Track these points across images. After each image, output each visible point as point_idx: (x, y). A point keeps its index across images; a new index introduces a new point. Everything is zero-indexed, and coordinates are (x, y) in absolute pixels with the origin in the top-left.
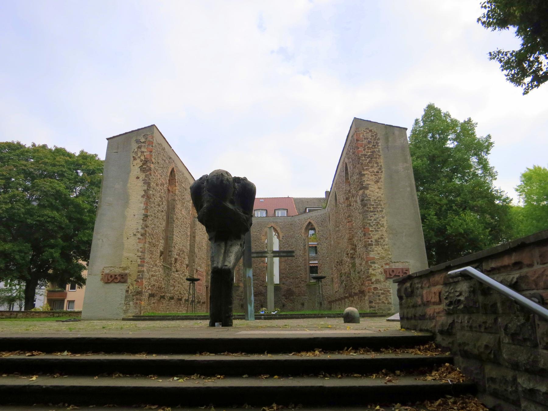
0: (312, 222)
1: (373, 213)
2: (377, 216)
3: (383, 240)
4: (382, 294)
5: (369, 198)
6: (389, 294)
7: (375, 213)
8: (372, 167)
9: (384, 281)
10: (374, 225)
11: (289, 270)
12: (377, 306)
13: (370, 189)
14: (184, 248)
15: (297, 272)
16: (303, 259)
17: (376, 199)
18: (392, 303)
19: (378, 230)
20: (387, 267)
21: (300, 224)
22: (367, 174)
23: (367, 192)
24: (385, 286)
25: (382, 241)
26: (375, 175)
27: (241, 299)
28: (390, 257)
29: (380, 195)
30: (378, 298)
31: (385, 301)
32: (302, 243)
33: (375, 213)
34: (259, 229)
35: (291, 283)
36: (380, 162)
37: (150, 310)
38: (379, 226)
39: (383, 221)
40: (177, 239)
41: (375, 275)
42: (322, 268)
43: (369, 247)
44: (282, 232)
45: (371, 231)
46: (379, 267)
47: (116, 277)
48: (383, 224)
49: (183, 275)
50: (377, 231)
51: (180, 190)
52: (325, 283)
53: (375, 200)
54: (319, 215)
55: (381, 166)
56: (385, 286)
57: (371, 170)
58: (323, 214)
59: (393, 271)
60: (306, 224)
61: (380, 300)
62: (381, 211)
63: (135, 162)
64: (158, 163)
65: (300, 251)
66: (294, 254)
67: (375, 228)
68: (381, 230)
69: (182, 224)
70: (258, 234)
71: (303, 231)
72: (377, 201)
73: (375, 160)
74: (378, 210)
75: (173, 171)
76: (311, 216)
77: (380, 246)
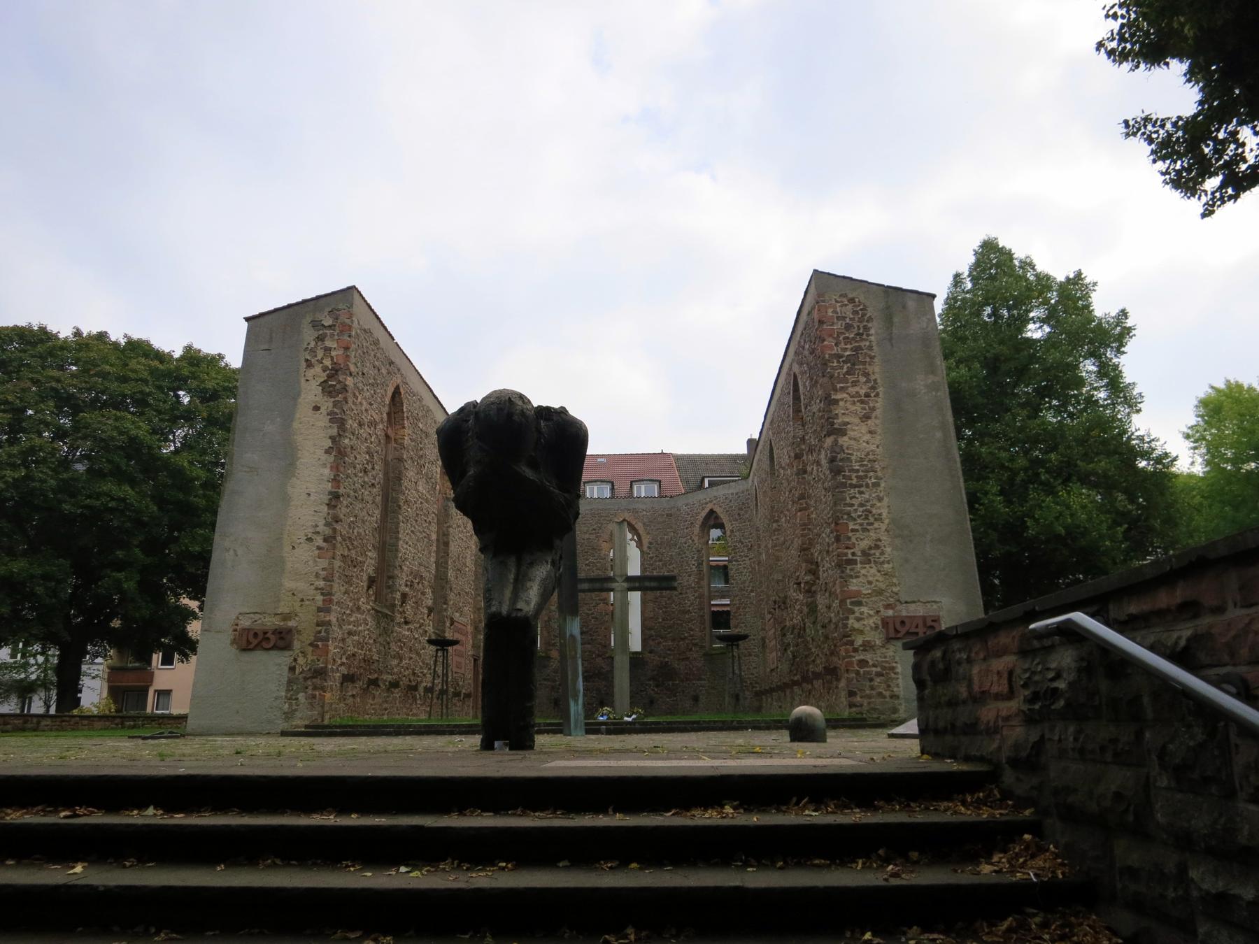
1: (857, 489)
2: (867, 496)
3: (879, 551)
4: (879, 674)
7: (862, 489)
8: (855, 384)
9: (883, 646)
10: (859, 516)
11: (663, 620)
12: (865, 702)
13: (852, 434)
15: (681, 625)
16: (696, 594)
17: (863, 456)
18: (901, 696)
19: (869, 527)
20: (890, 613)
22: (842, 399)
23: (844, 441)
24: (885, 657)
25: (877, 554)
26: (862, 402)
27: (553, 688)
28: (895, 590)
29: (873, 447)
31: (884, 692)
32: (693, 558)
33: (862, 489)
35: (669, 650)
36: (873, 373)
38: (872, 520)
39: (879, 508)
41: (861, 632)
42: (740, 615)
44: (648, 534)
45: (853, 530)
46: (871, 612)
48: (880, 514)
50: (865, 530)
51: (414, 436)
52: (746, 649)
53: (862, 460)
54: (732, 494)
55: (875, 380)
57: (852, 390)
58: (743, 492)
59: (903, 623)
60: (704, 514)
61: (872, 688)
62: (876, 485)
63: (310, 373)
65: (690, 576)
66: (676, 584)
67: (861, 524)
68: (876, 529)
69: (417, 515)
70: (593, 537)
71: (697, 530)
72: (865, 463)
73: (861, 367)
77: (873, 565)
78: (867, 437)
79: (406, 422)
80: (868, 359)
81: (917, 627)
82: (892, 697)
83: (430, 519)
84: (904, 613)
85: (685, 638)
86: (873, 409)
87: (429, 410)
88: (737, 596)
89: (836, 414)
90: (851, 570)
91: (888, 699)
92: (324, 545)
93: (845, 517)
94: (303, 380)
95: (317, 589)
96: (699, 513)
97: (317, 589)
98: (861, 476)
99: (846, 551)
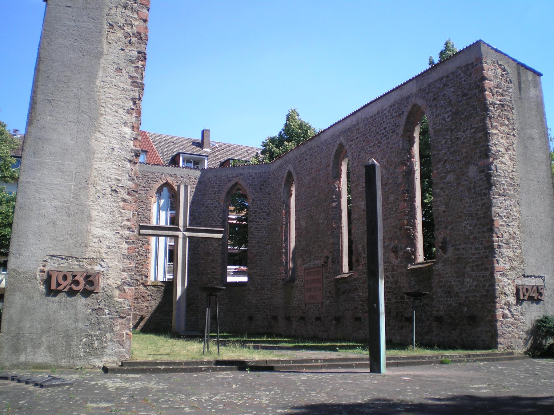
0: (241, 182)
21: (216, 184)
22: (495, 134)
32: (218, 216)
33: (506, 198)
34: (144, 185)
35: (194, 281)
42: (257, 260)
45: (502, 225)
47: (76, 278)
54: (256, 173)
58: (265, 173)
60: (230, 185)
76: (241, 173)
84: (527, 283)
85: (208, 273)
88: (255, 246)
92: (127, 197)
94: (105, 41)
95: (122, 237)
96: (226, 184)
97: (122, 237)
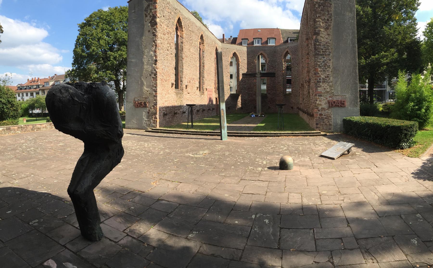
1: (322, 56)
2: (325, 59)
3: (328, 78)
4: (326, 118)
5: (320, 43)
6: (330, 118)
7: (324, 56)
8: (324, 15)
9: (328, 109)
10: (322, 66)
12: (321, 126)
13: (321, 35)
14: (194, 76)
17: (325, 44)
18: (332, 125)
19: (325, 70)
20: (331, 99)
22: (318, 21)
23: (319, 37)
24: (328, 113)
25: (328, 79)
26: (326, 22)
28: (333, 91)
29: (328, 40)
30: (322, 121)
31: (327, 124)
33: (324, 56)
36: (331, 11)
37: (165, 123)
38: (327, 67)
39: (329, 63)
40: (187, 71)
41: (321, 105)
43: (318, 84)
44: (268, 58)
46: (324, 99)
48: (330, 66)
49: (194, 94)
50: (324, 71)
51: (188, 33)
53: (324, 45)
54: (293, 46)
55: (331, 14)
56: (328, 113)
57: (323, 17)
58: (296, 46)
59: (334, 102)
60: (285, 52)
61: (323, 122)
62: (329, 55)
63: (147, 18)
64: (164, 16)
65: (280, 72)
67: (323, 69)
68: (328, 71)
69: (191, 60)
72: (325, 46)
73: (326, 8)
74: (327, 54)
75: (179, 19)
77: (326, 83)
78: (327, 36)
79: (183, 29)
80: (329, 5)
81: (338, 104)
82: (329, 125)
83: (196, 60)
85: (279, 90)
86: (330, 26)
87: (193, 23)
89: (317, 27)
90: (319, 84)
91: (328, 126)
93: (318, 66)
94: (145, 21)
97: (153, 90)
98: (324, 51)
99: (317, 78)
